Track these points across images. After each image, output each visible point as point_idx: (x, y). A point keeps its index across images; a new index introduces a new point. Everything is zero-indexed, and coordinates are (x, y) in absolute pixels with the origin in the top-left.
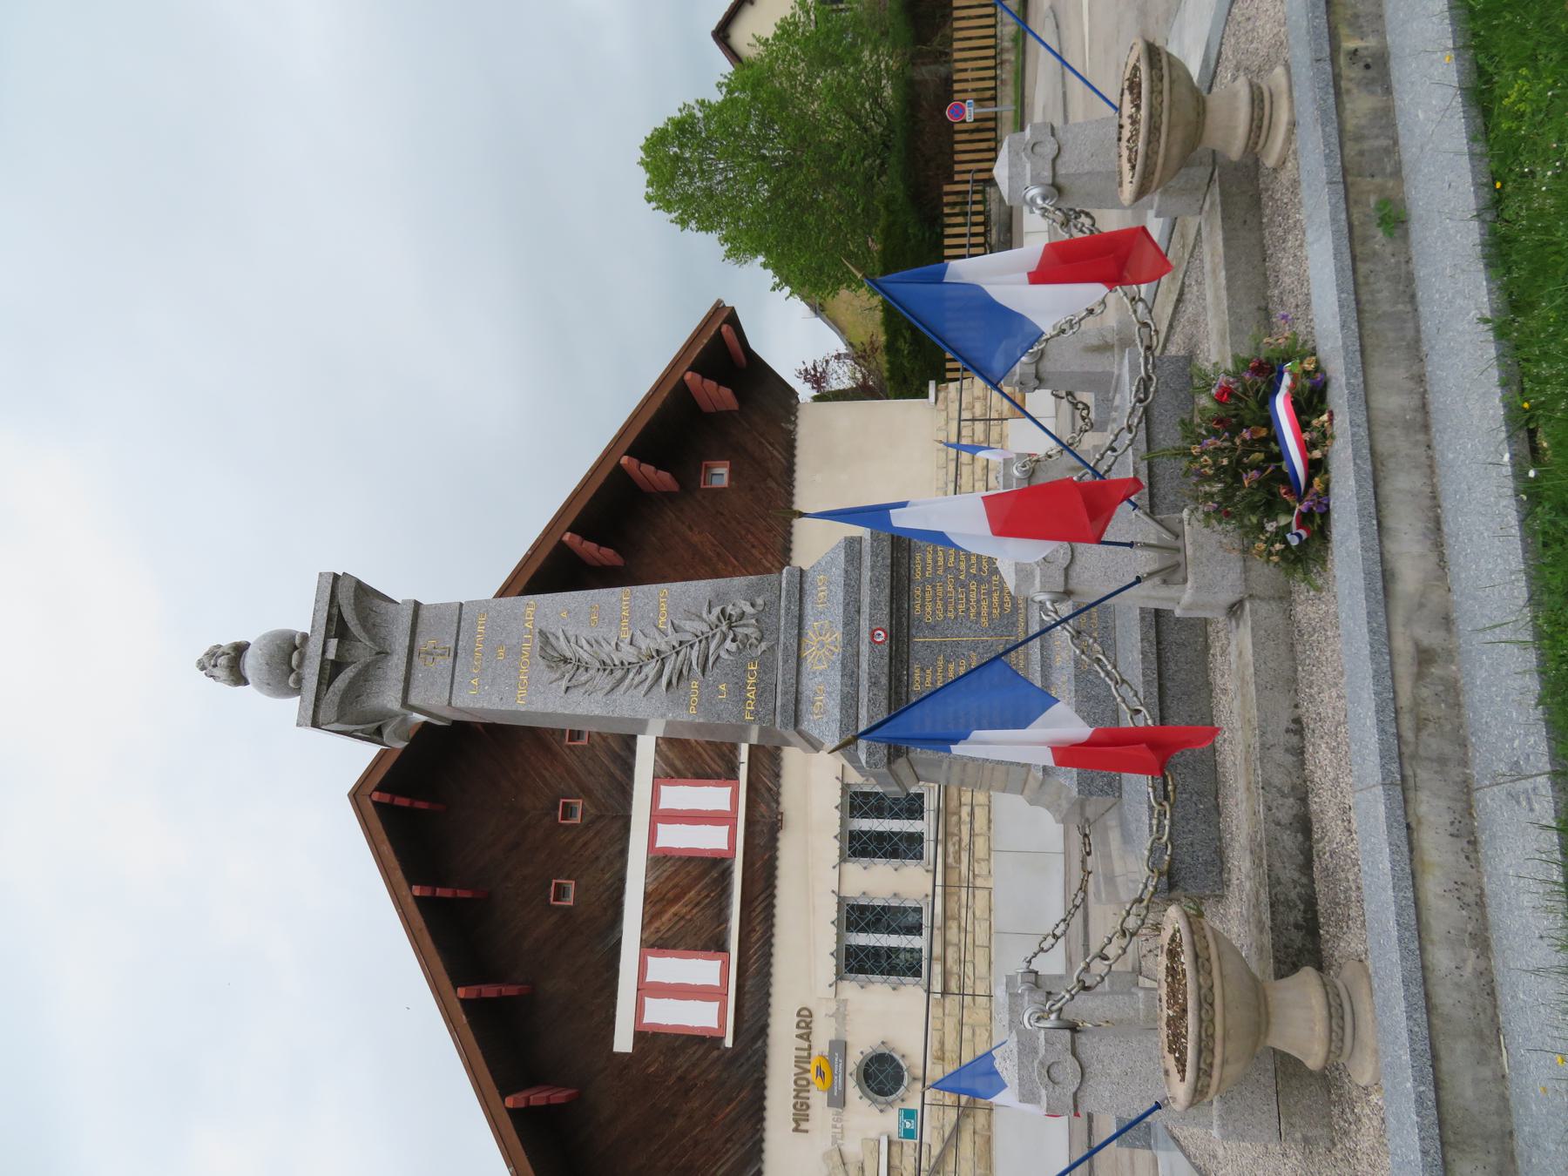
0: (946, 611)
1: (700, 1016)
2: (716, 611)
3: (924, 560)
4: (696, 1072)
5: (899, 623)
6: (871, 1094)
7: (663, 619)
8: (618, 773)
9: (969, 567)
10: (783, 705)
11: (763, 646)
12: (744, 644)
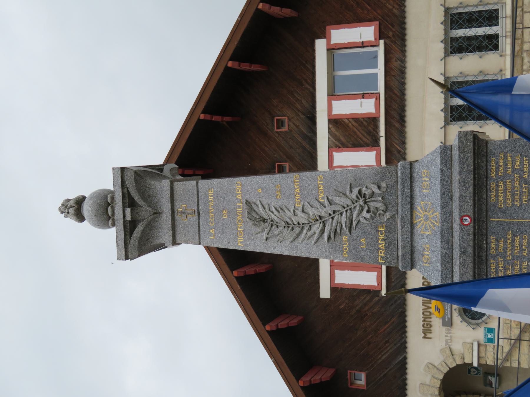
0: (513, 200)
1: (366, 279)
2: (356, 191)
3: (497, 163)
4: (366, 308)
5: (480, 209)
6: (467, 319)
7: (322, 195)
8: (307, 146)
10: (403, 255)
11: (388, 215)
12: (374, 213)
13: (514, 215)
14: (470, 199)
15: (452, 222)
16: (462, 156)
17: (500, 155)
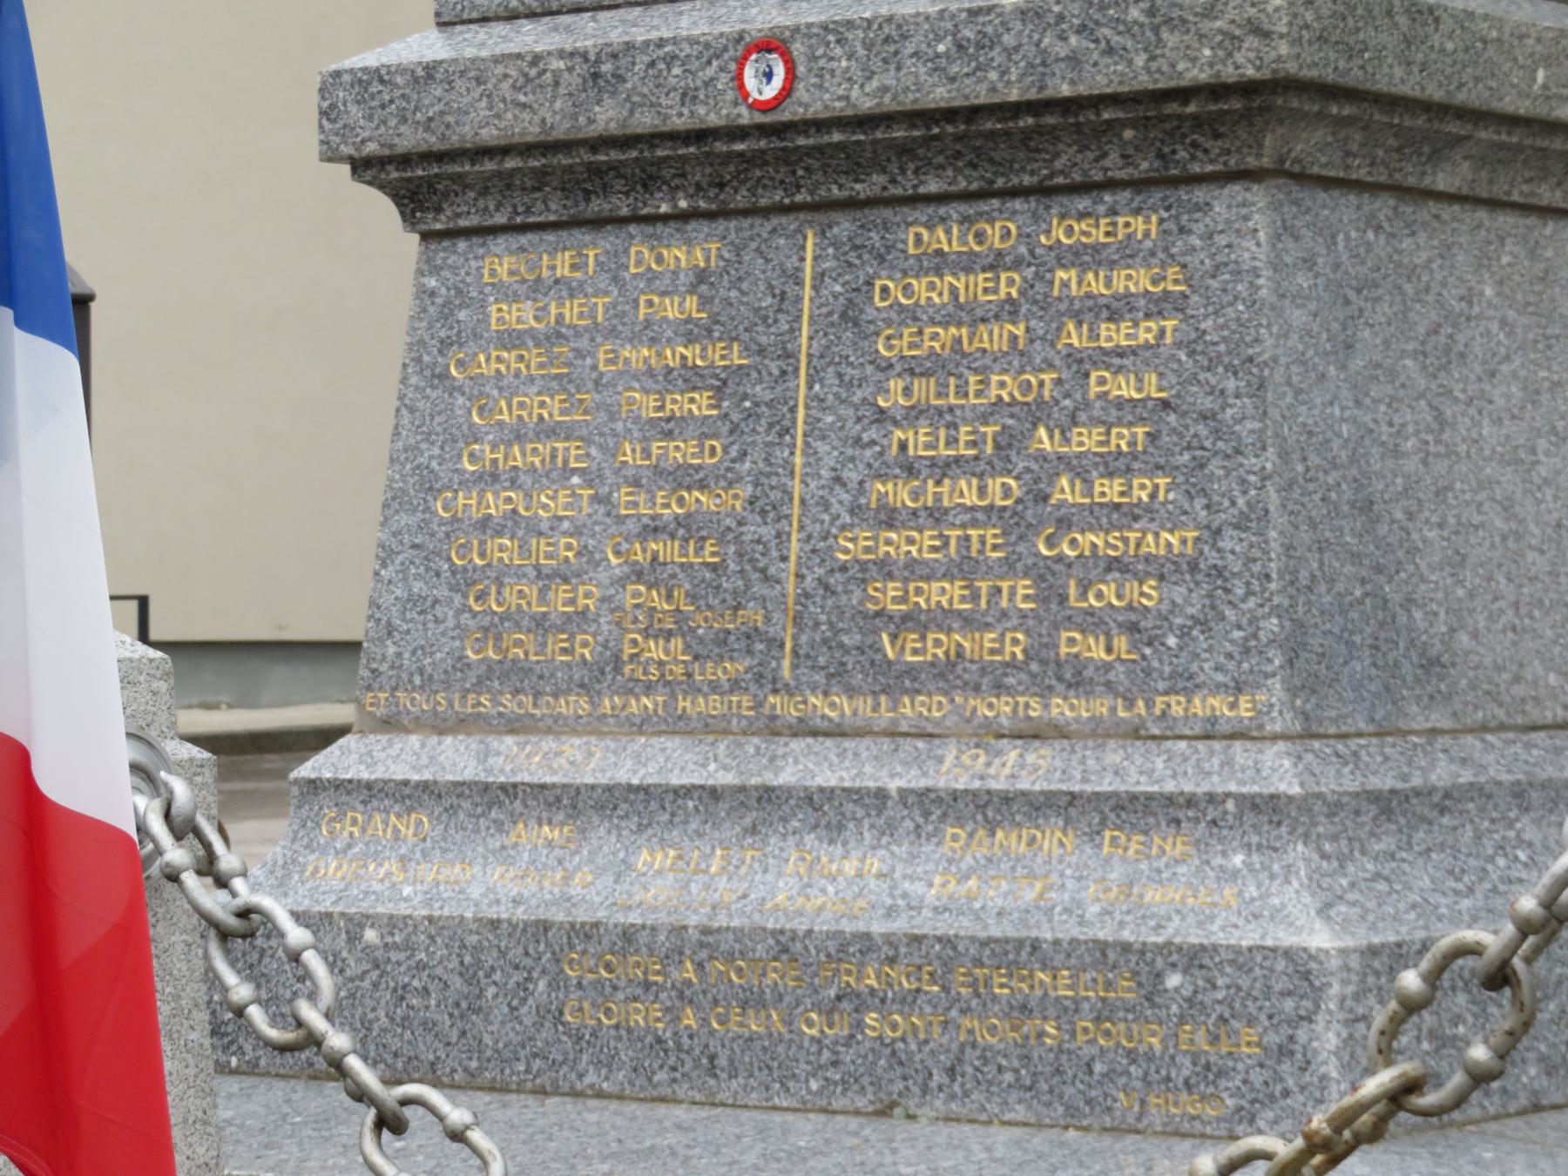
0: (912, 370)
3: (1128, 253)
5: (855, 162)
9: (1079, 468)
13: (831, 379)
14: (884, 89)
17: (1172, 272)
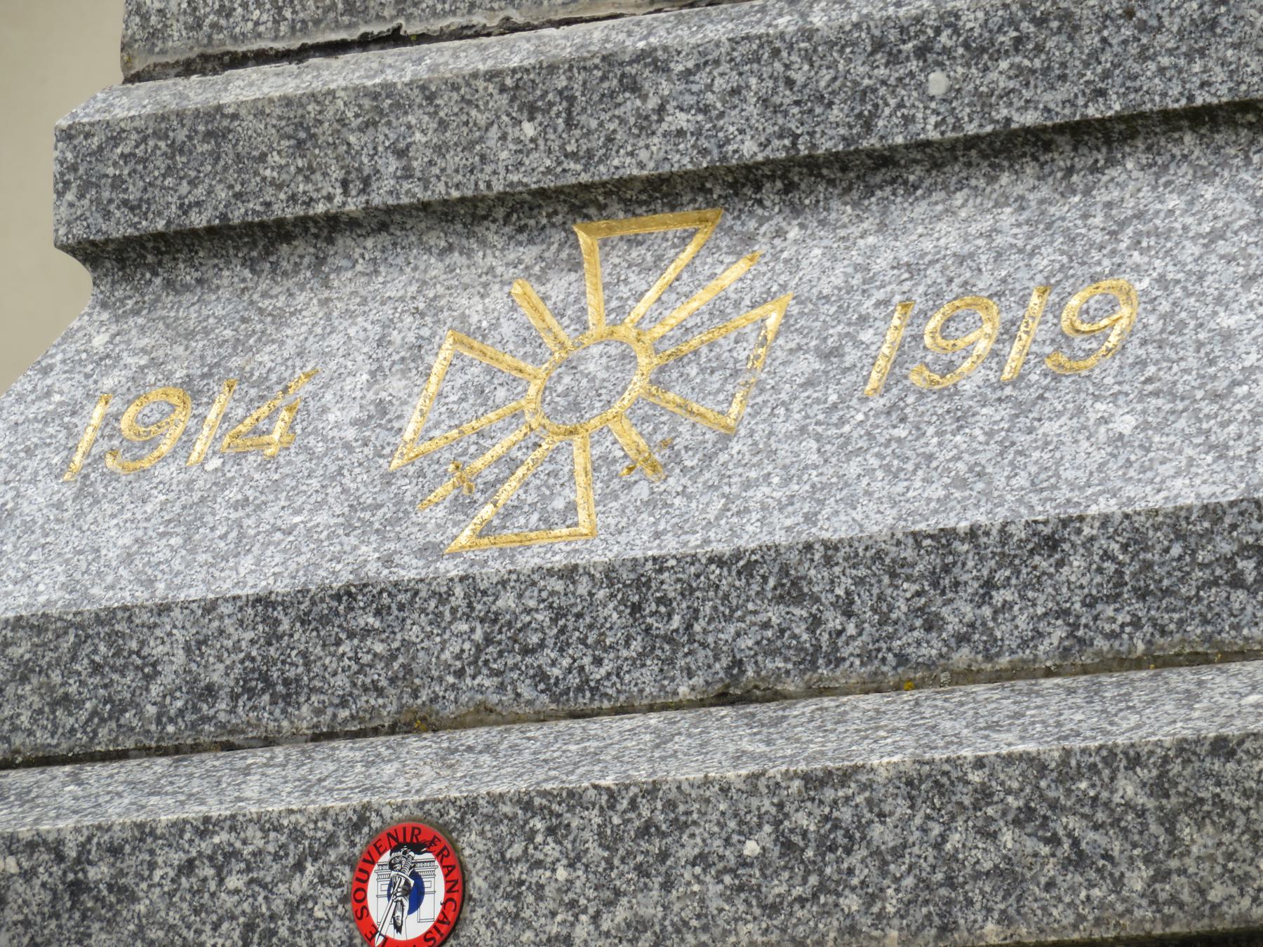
10: (216, 125)
15: (483, 715)
16: (1127, 788)
